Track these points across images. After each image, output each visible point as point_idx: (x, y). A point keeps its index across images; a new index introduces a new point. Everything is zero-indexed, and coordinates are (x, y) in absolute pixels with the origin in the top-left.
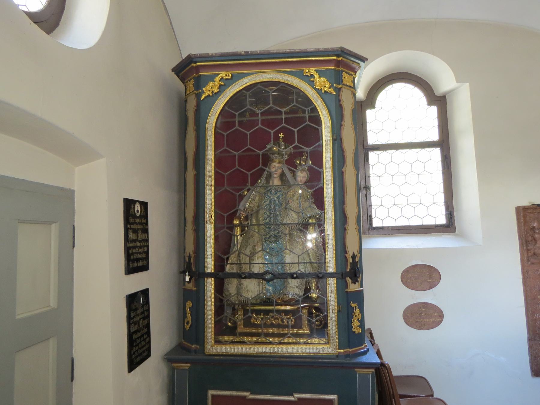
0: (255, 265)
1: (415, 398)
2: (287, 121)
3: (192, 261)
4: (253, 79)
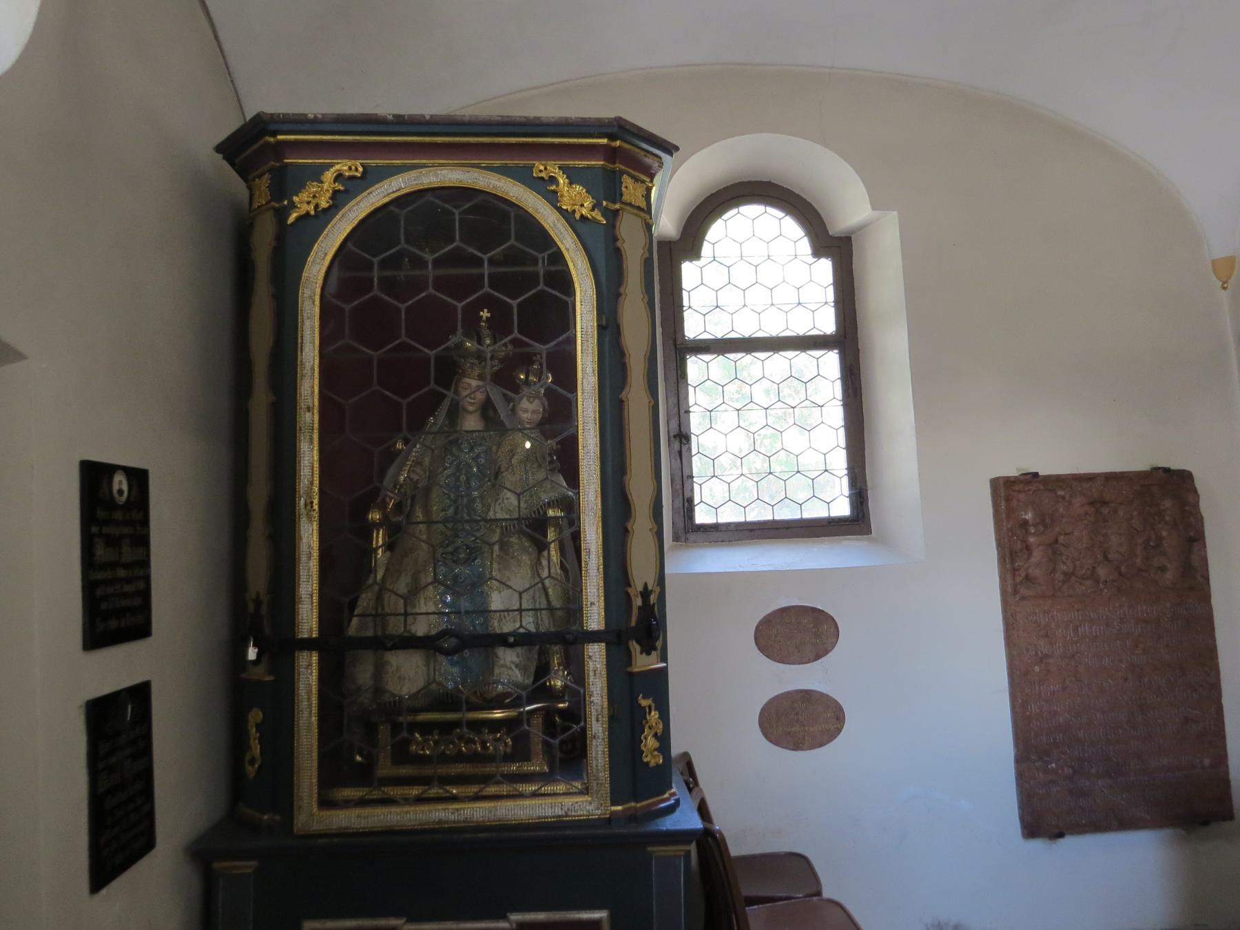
0: (419, 617)
1: (781, 903)
2: (496, 282)
3: (264, 610)
4: (415, 180)
